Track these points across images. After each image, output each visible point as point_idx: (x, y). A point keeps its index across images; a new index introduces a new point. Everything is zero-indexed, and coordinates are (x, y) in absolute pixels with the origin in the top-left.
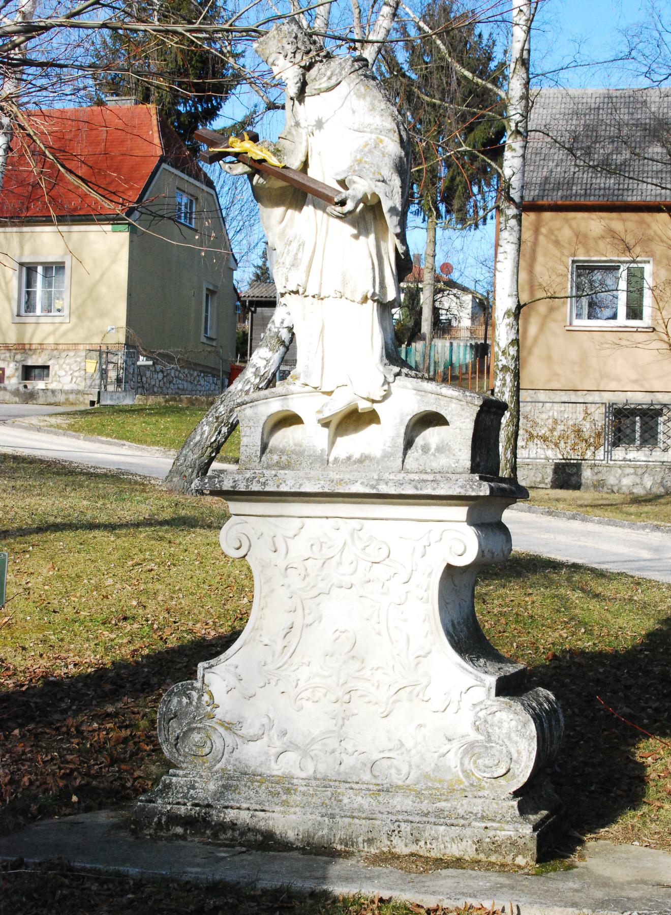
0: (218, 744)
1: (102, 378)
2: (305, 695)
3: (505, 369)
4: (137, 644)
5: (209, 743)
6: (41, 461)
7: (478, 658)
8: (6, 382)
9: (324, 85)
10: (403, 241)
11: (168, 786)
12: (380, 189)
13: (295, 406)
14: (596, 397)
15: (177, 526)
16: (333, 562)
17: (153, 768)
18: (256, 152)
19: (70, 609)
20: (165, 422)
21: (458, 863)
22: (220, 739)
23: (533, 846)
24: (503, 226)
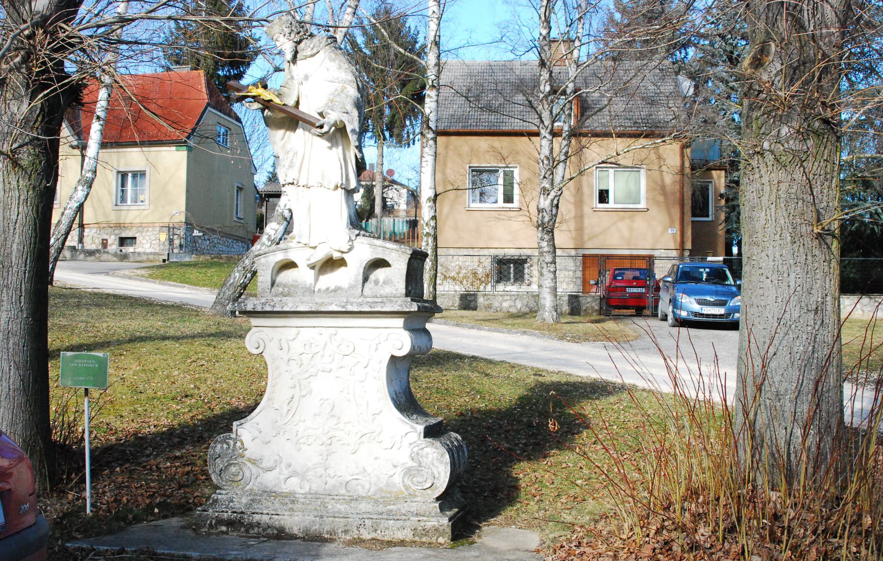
0: (247, 474)
1: (170, 245)
2: (302, 441)
3: (428, 234)
4: (195, 412)
5: (241, 473)
6: (131, 298)
7: (412, 414)
8: (109, 248)
9: (309, 53)
10: (361, 151)
11: (216, 501)
12: (345, 118)
13: (293, 256)
14: (486, 252)
15: (219, 337)
16: (319, 355)
17: (206, 491)
18: (266, 95)
19: (151, 391)
20: (211, 271)
21: (402, 543)
22: (249, 470)
23: (449, 531)
24: (425, 145)
